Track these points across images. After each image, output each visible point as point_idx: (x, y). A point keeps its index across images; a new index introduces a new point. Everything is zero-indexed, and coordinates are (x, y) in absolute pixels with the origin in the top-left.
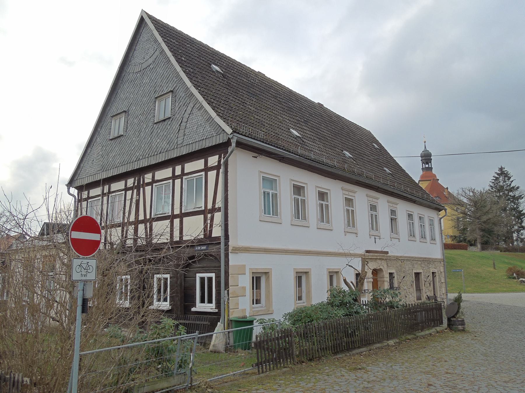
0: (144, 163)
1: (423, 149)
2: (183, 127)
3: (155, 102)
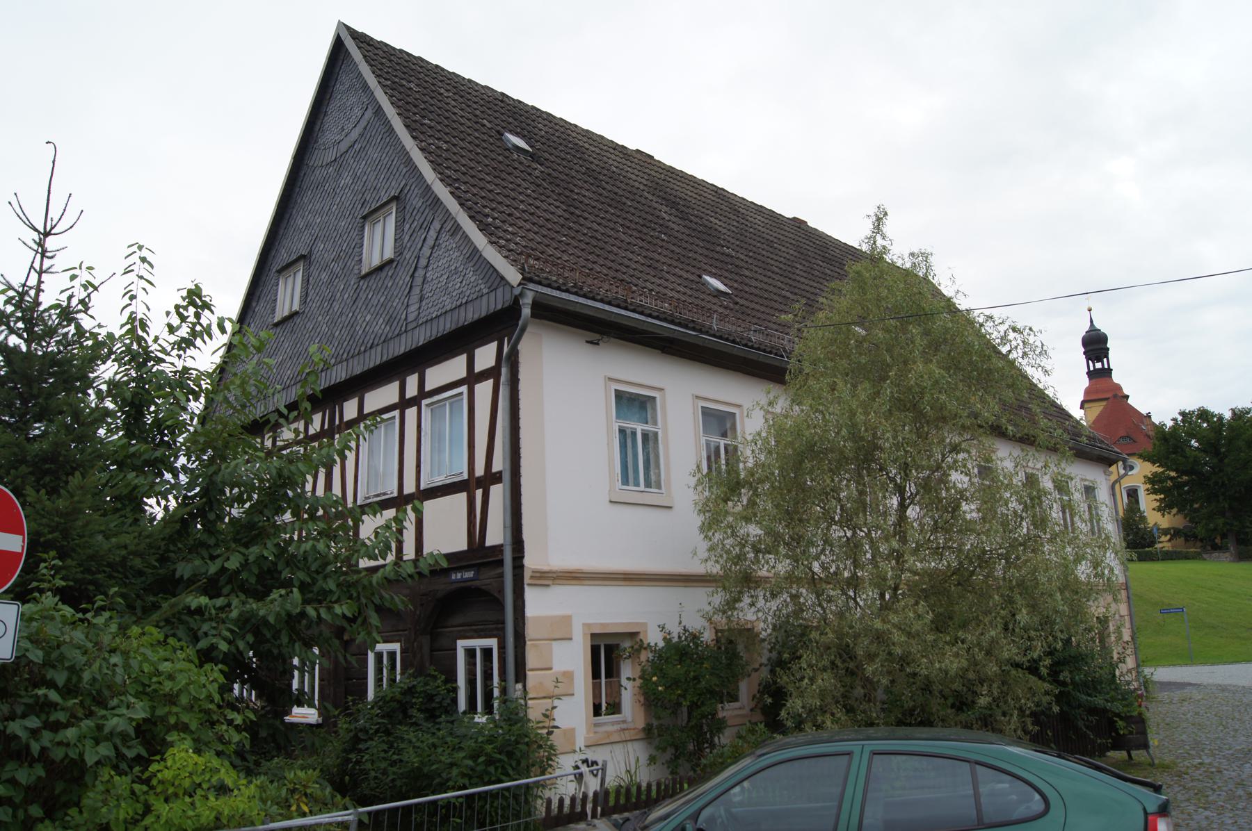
0: (339, 374)
1: (1087, 327)
2: (418, 281)
3: (363, 227)
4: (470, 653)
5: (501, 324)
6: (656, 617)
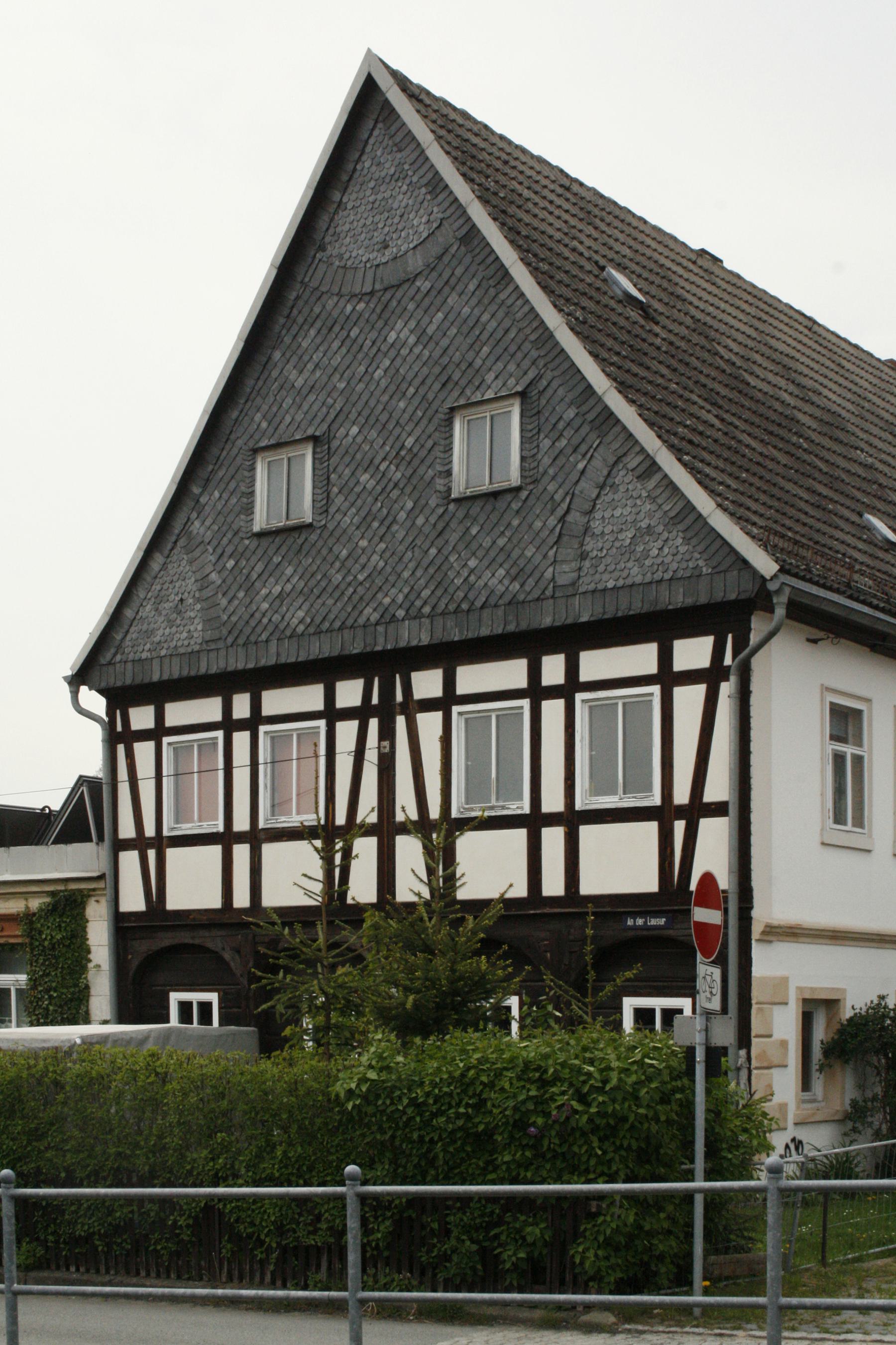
5: (730, 615)
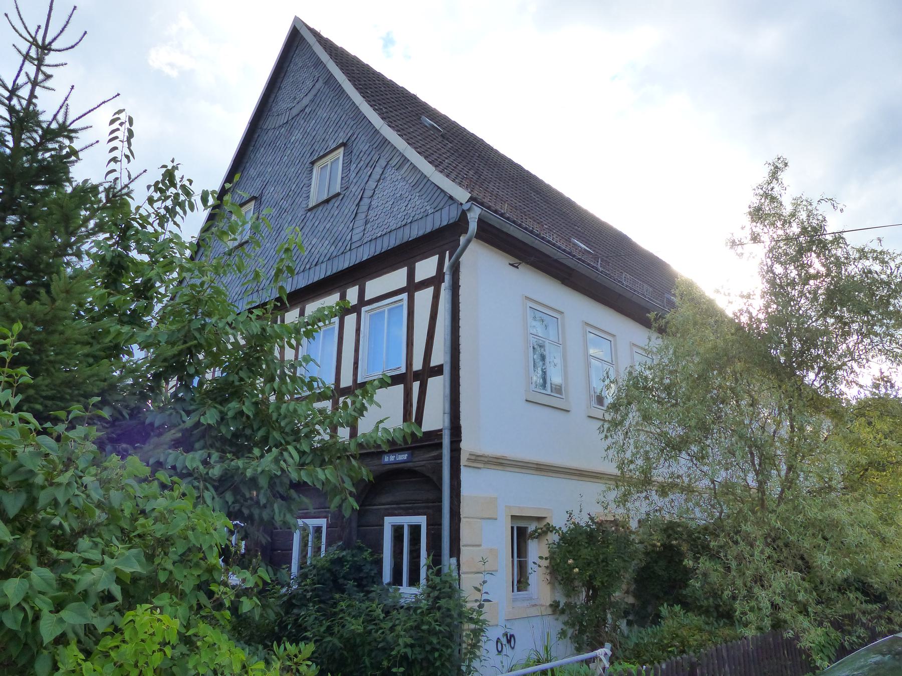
3: (311, 171)
4: (398, 531)
5: (443, 239)
6: (571, 505)
